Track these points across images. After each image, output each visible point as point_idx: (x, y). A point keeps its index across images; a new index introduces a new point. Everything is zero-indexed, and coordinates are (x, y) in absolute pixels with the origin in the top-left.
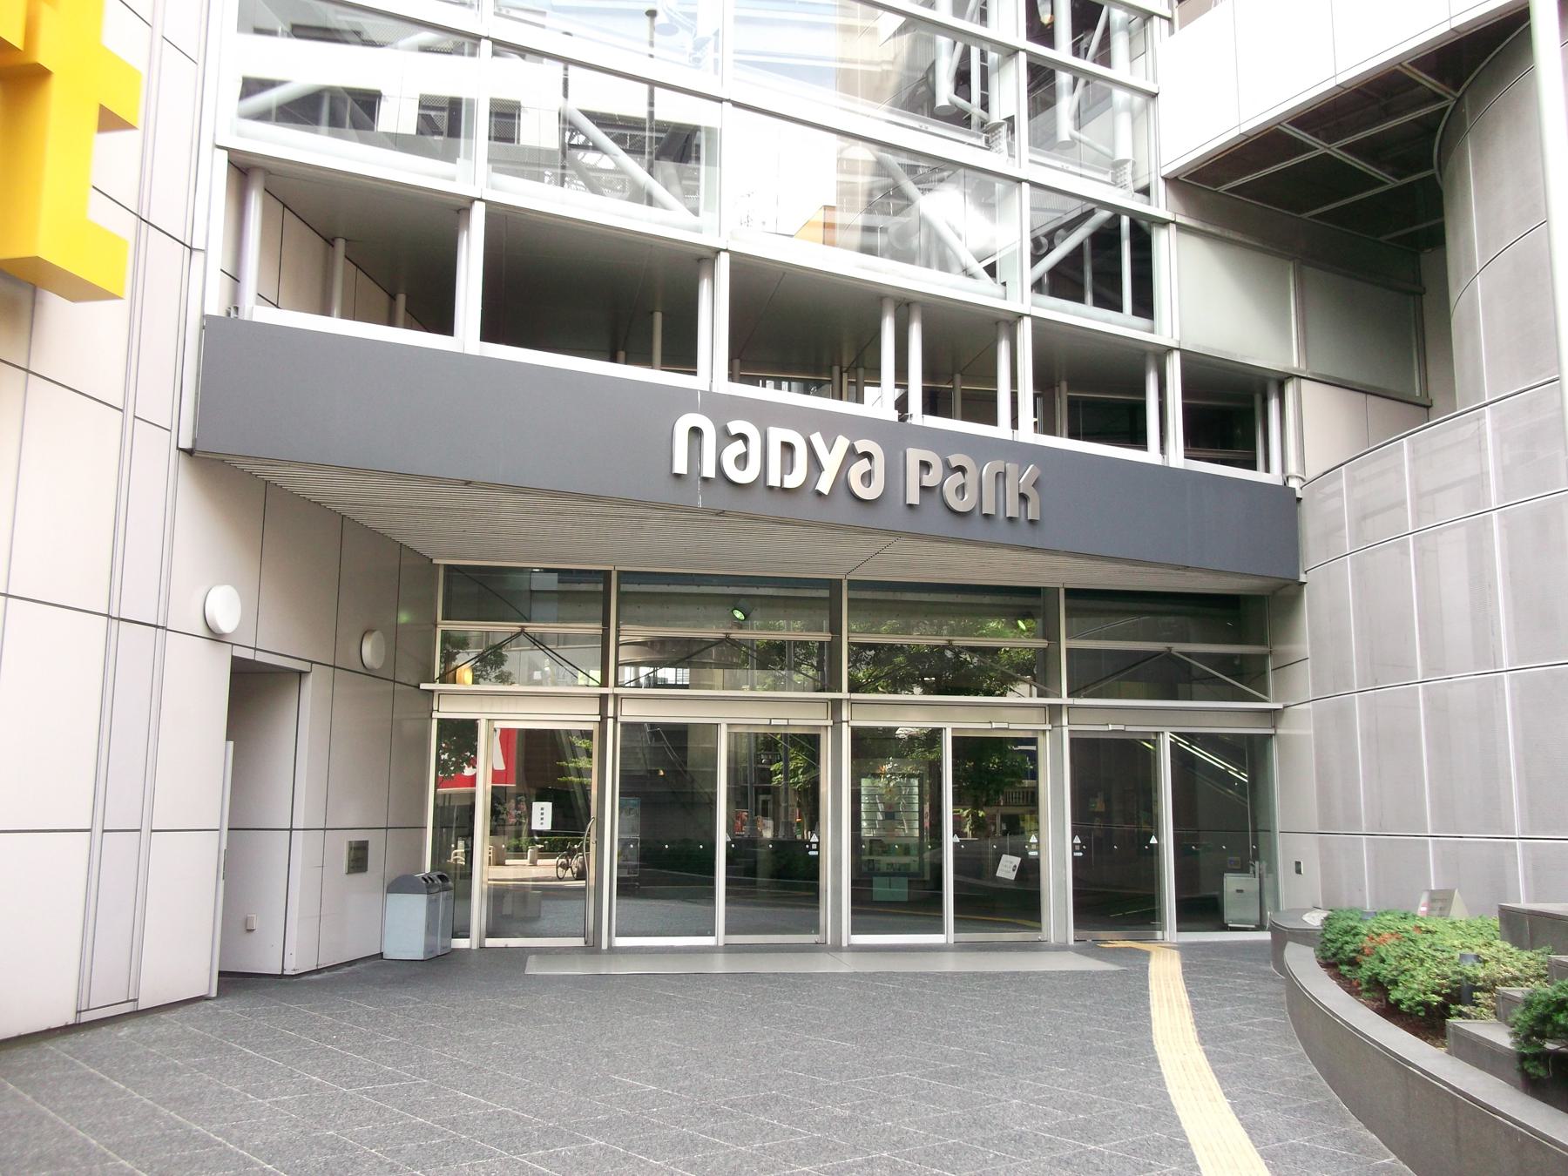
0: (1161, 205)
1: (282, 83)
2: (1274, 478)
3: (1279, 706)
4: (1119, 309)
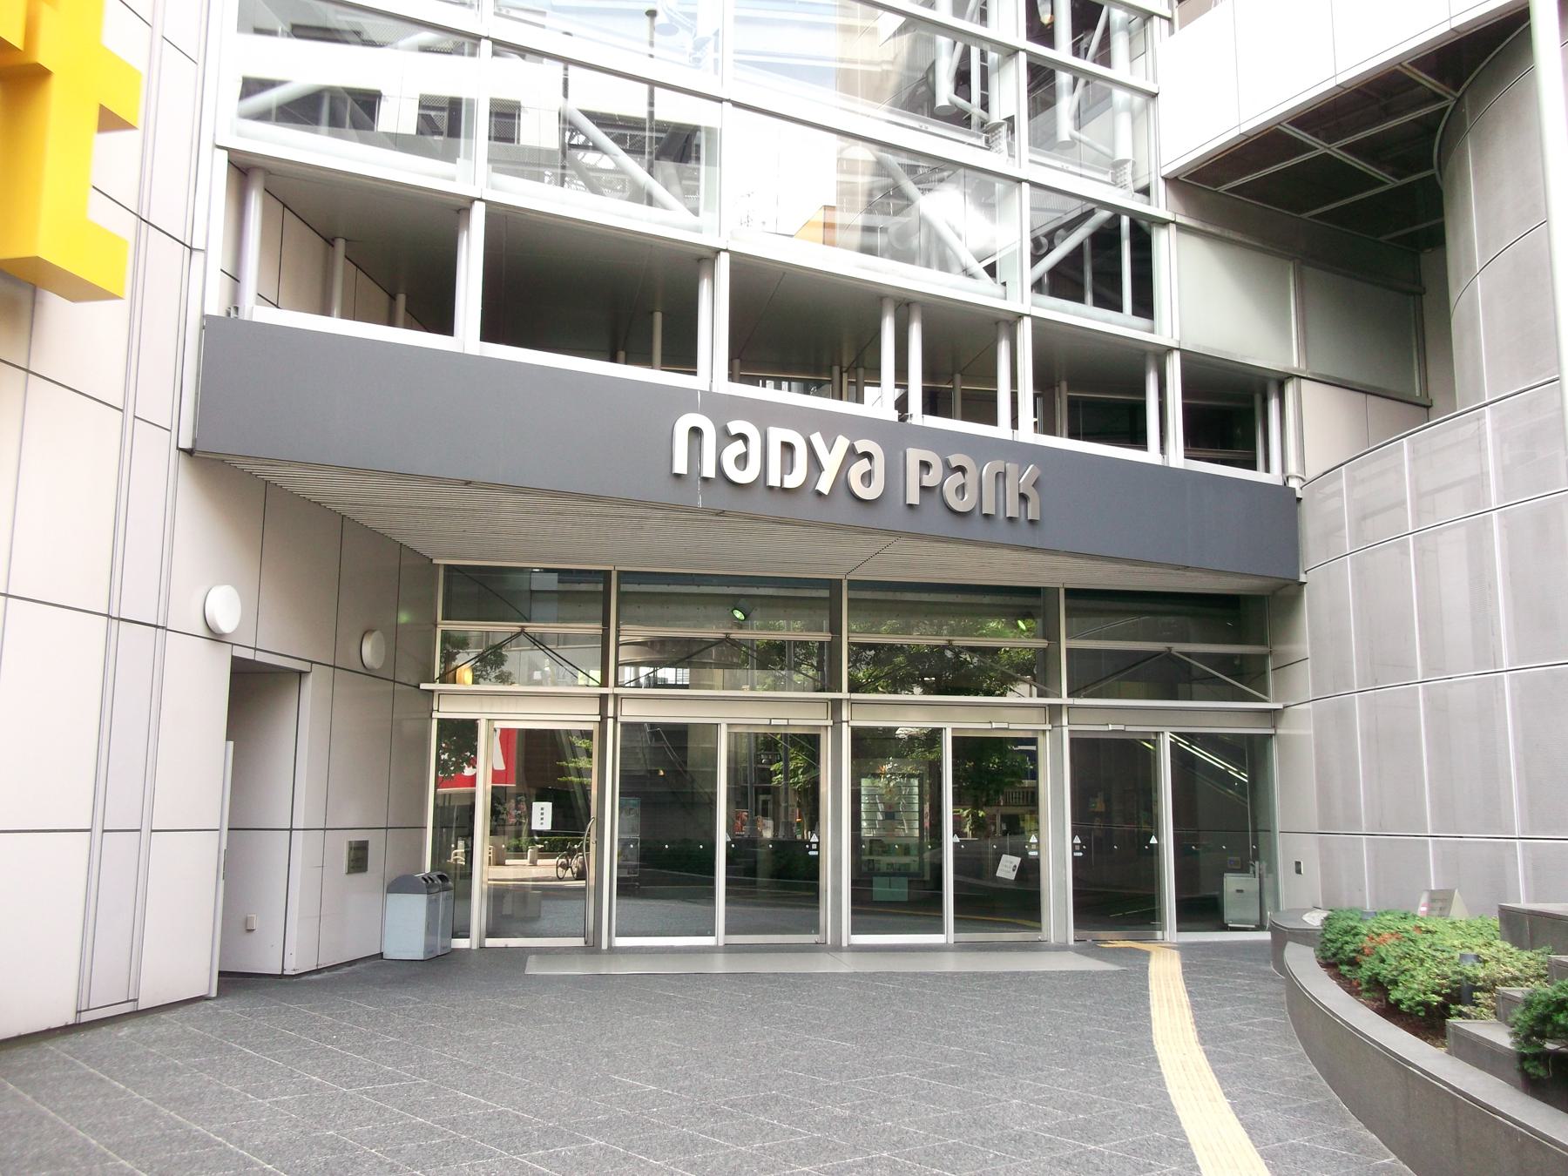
0: (1161, 205)
2: (1274, 477)
3: (1280, 706)
4: (1119, 309)
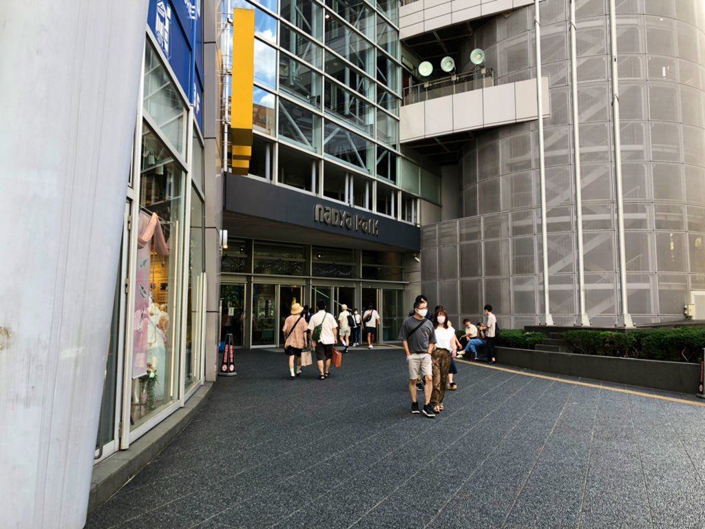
0: (398, 152)
1: (147, 33)
2: (412, 223)
3: (408, 282)
4: (387, 177)
